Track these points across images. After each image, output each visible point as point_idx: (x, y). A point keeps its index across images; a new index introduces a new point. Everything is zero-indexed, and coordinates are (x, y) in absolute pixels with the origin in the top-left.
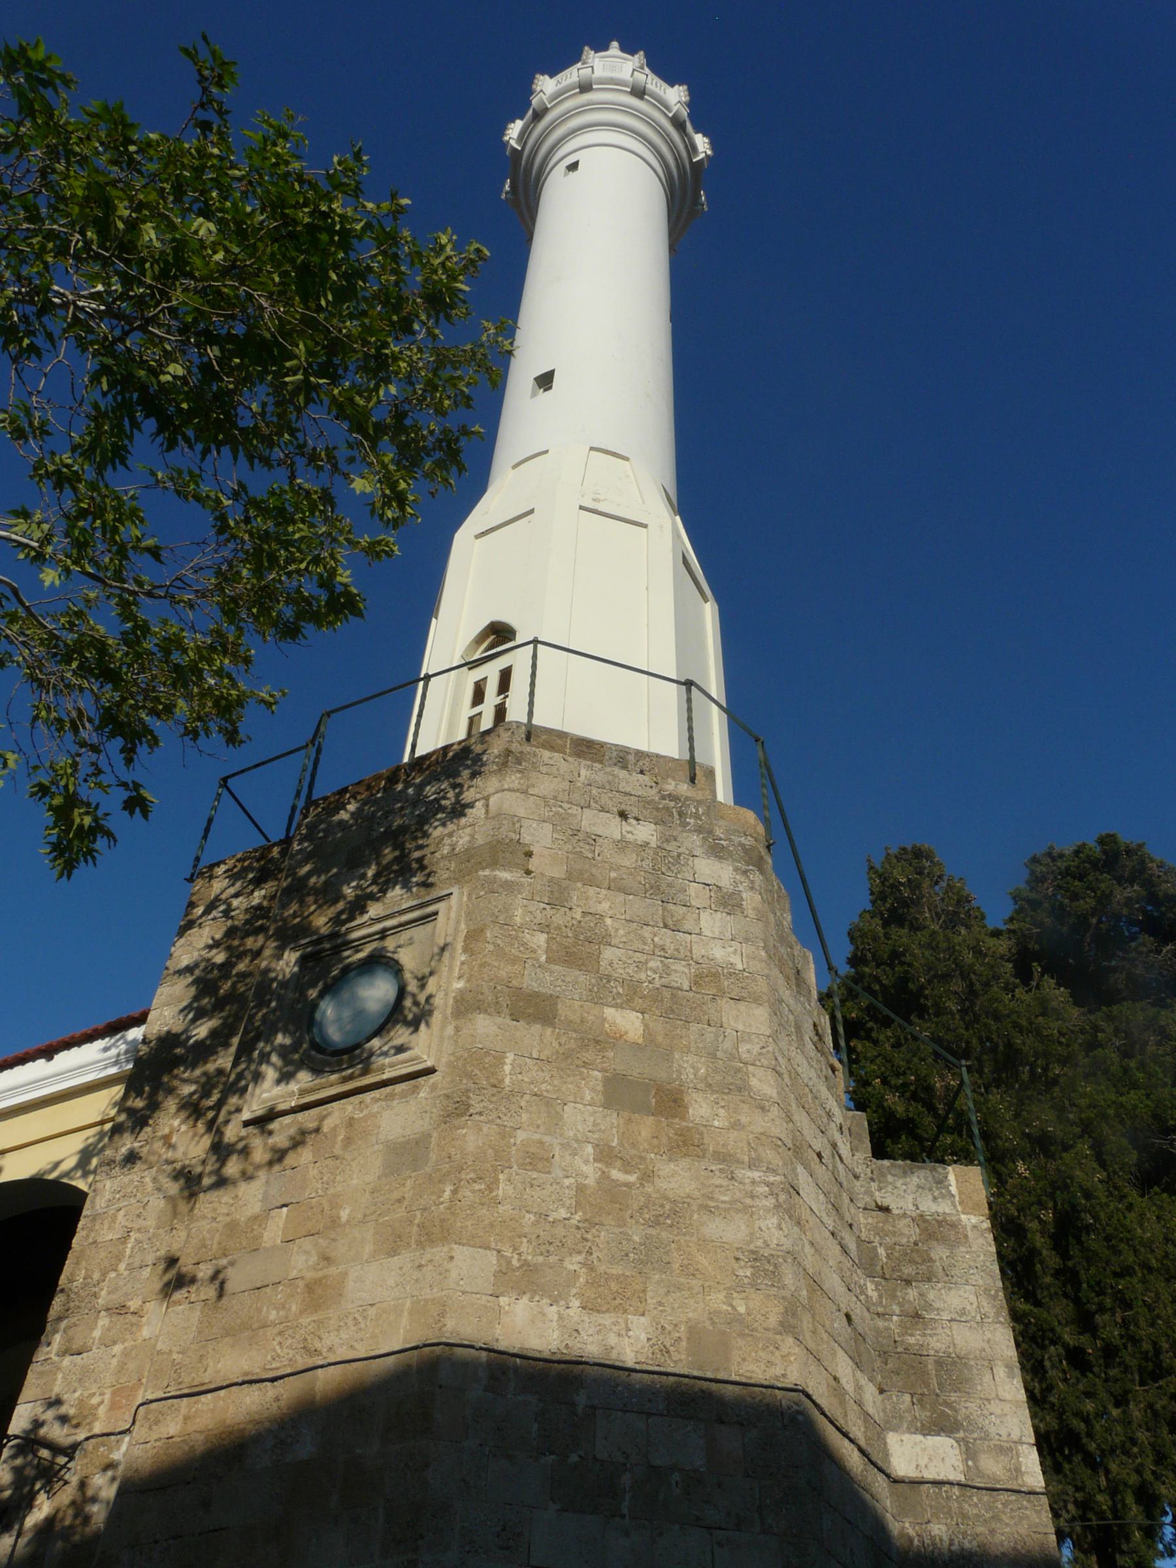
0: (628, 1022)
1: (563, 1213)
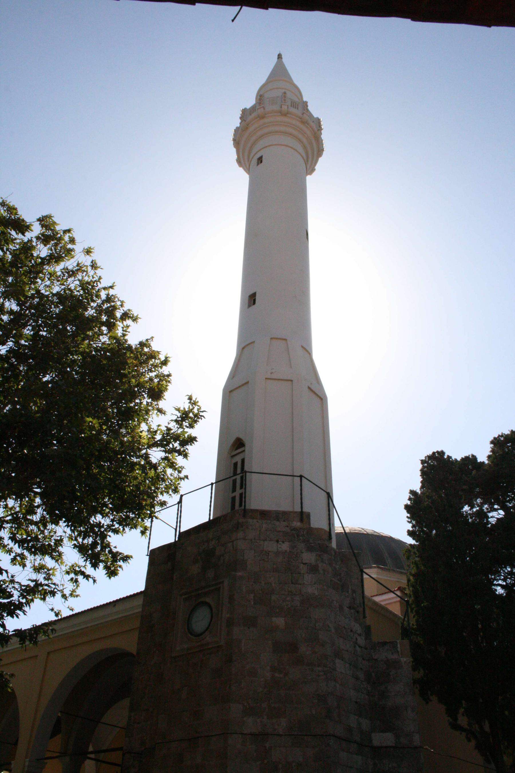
0: (280, 621)
1: (261, 689)
